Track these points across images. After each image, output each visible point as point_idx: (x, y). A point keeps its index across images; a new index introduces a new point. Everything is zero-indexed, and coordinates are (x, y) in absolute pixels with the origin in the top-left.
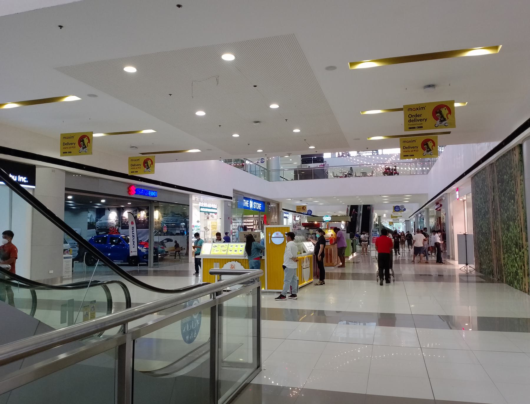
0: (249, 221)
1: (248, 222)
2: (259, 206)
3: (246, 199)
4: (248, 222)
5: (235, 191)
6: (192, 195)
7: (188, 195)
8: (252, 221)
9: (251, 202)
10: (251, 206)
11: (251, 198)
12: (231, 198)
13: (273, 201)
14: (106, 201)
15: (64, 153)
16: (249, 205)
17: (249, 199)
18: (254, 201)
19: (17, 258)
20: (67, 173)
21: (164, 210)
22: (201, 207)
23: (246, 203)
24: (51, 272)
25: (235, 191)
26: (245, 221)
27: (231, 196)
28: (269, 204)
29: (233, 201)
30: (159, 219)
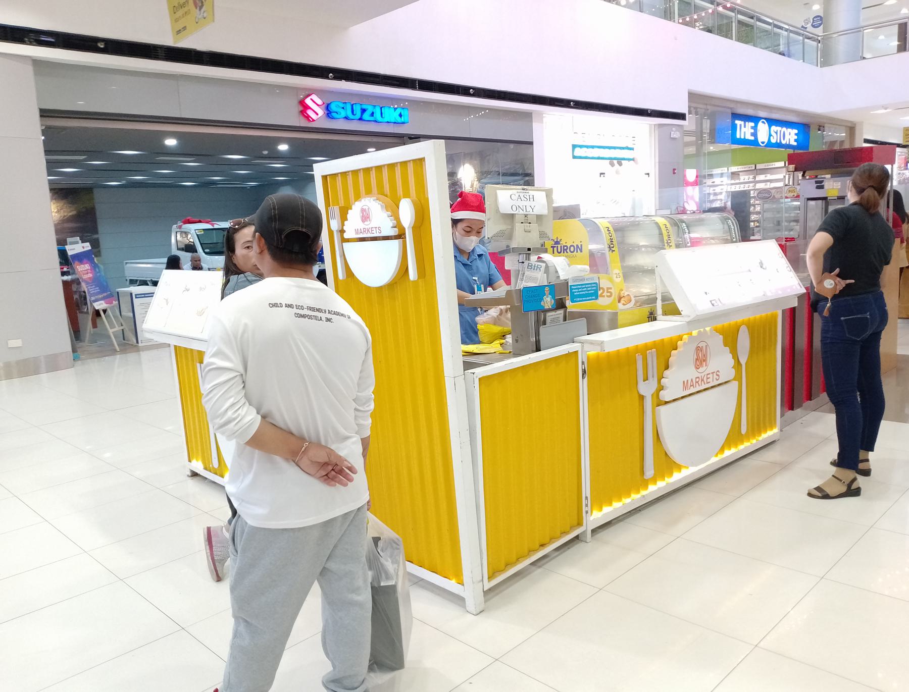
0: (769, 177)
1: (771, 181)
2: (791, 136)
3: (746, 118)
4: (771, 181)
5: (693, 97)
6: (540, 115)
7: (528, 115)
8: (781, 176)
9: (763, 127)
10: (763, 137)
11: (762, 114)
12: (681, 116)
13: (835, 122)
14: (180, 144)
15: (871, 148)
16: (755, 134)
17: (755, 119)
18: (771, 122)
19: (888, 263)
20: (37, 63)
21: (482, 162)
22: (574, 146)
23: (745, 130)
24: (15, 343)
25: (693, 97)
26: (761, 177)
27: (683, 108)
28: (821, 127)
29: (688, 124)
30: (472, 186)
